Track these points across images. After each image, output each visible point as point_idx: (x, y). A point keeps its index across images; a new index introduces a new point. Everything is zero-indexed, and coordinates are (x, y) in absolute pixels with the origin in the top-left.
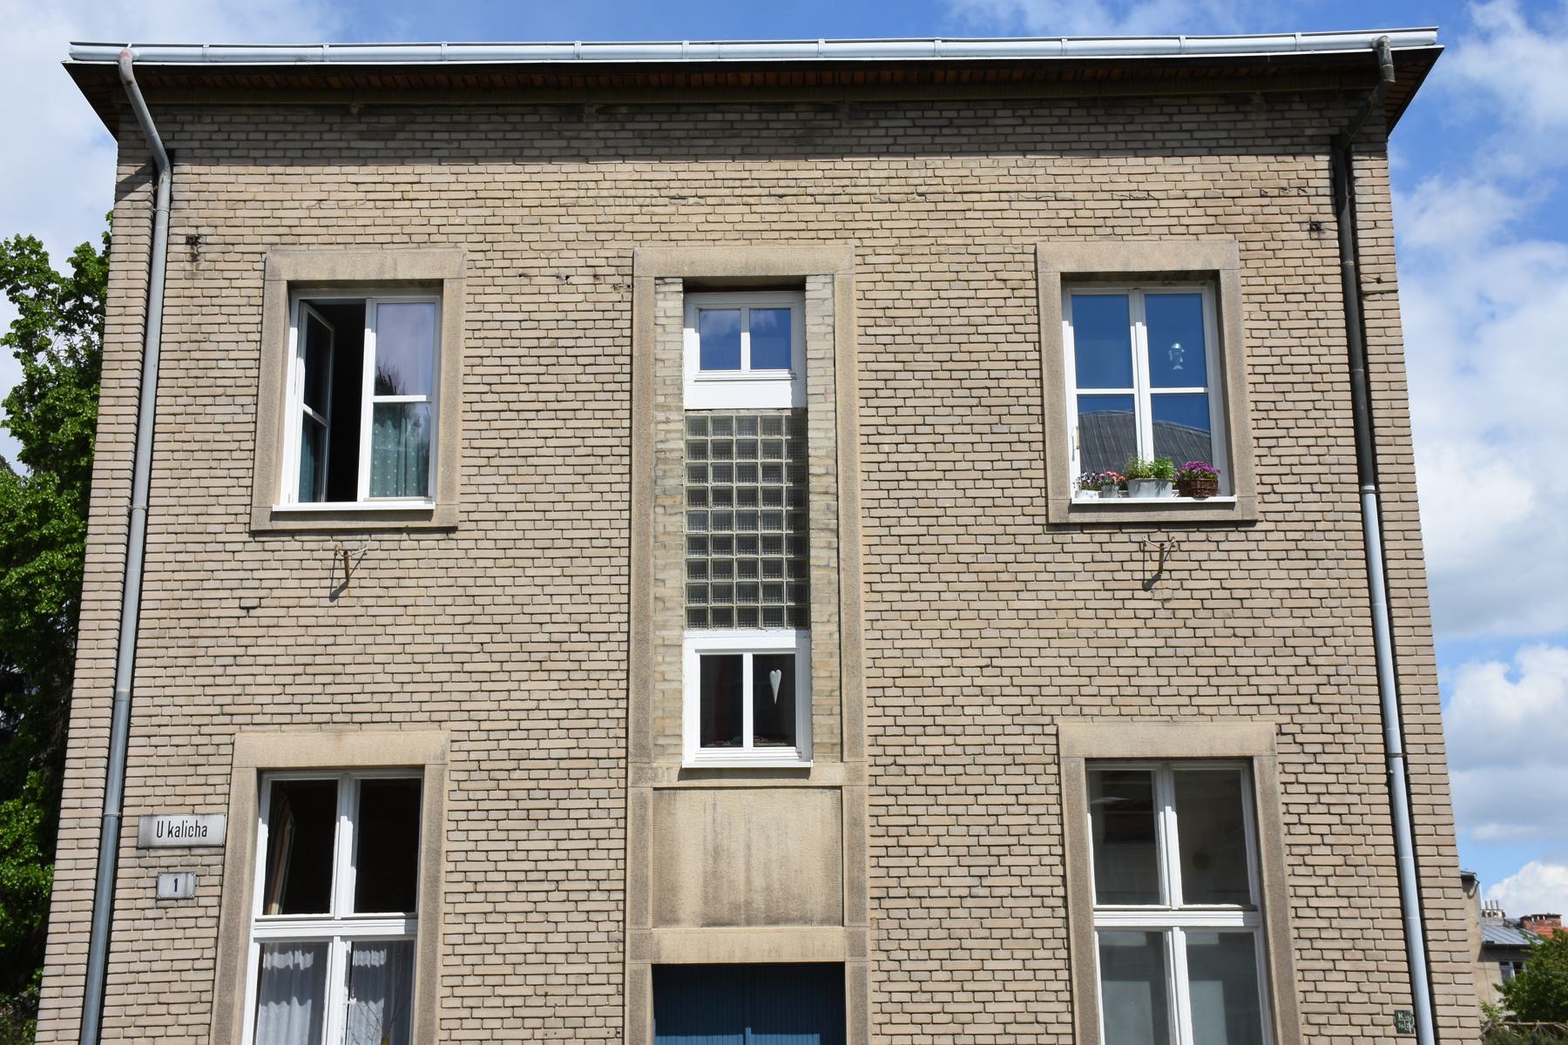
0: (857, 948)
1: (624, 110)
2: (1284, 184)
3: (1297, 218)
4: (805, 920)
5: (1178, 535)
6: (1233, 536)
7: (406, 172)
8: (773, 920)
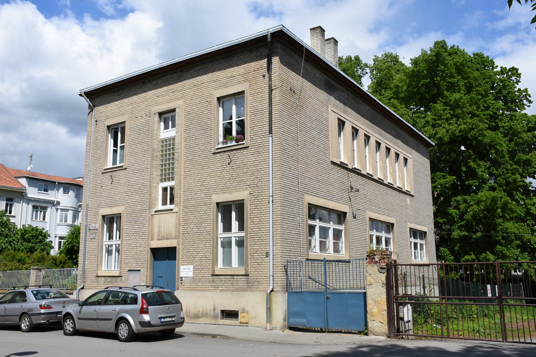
0: (179, 244)
2: (258, 67)
3: (260, 75)
4: (172, 239)
5: (235, 152)
6: (245, 151)
7: (122, 101)
8: (167, 239)
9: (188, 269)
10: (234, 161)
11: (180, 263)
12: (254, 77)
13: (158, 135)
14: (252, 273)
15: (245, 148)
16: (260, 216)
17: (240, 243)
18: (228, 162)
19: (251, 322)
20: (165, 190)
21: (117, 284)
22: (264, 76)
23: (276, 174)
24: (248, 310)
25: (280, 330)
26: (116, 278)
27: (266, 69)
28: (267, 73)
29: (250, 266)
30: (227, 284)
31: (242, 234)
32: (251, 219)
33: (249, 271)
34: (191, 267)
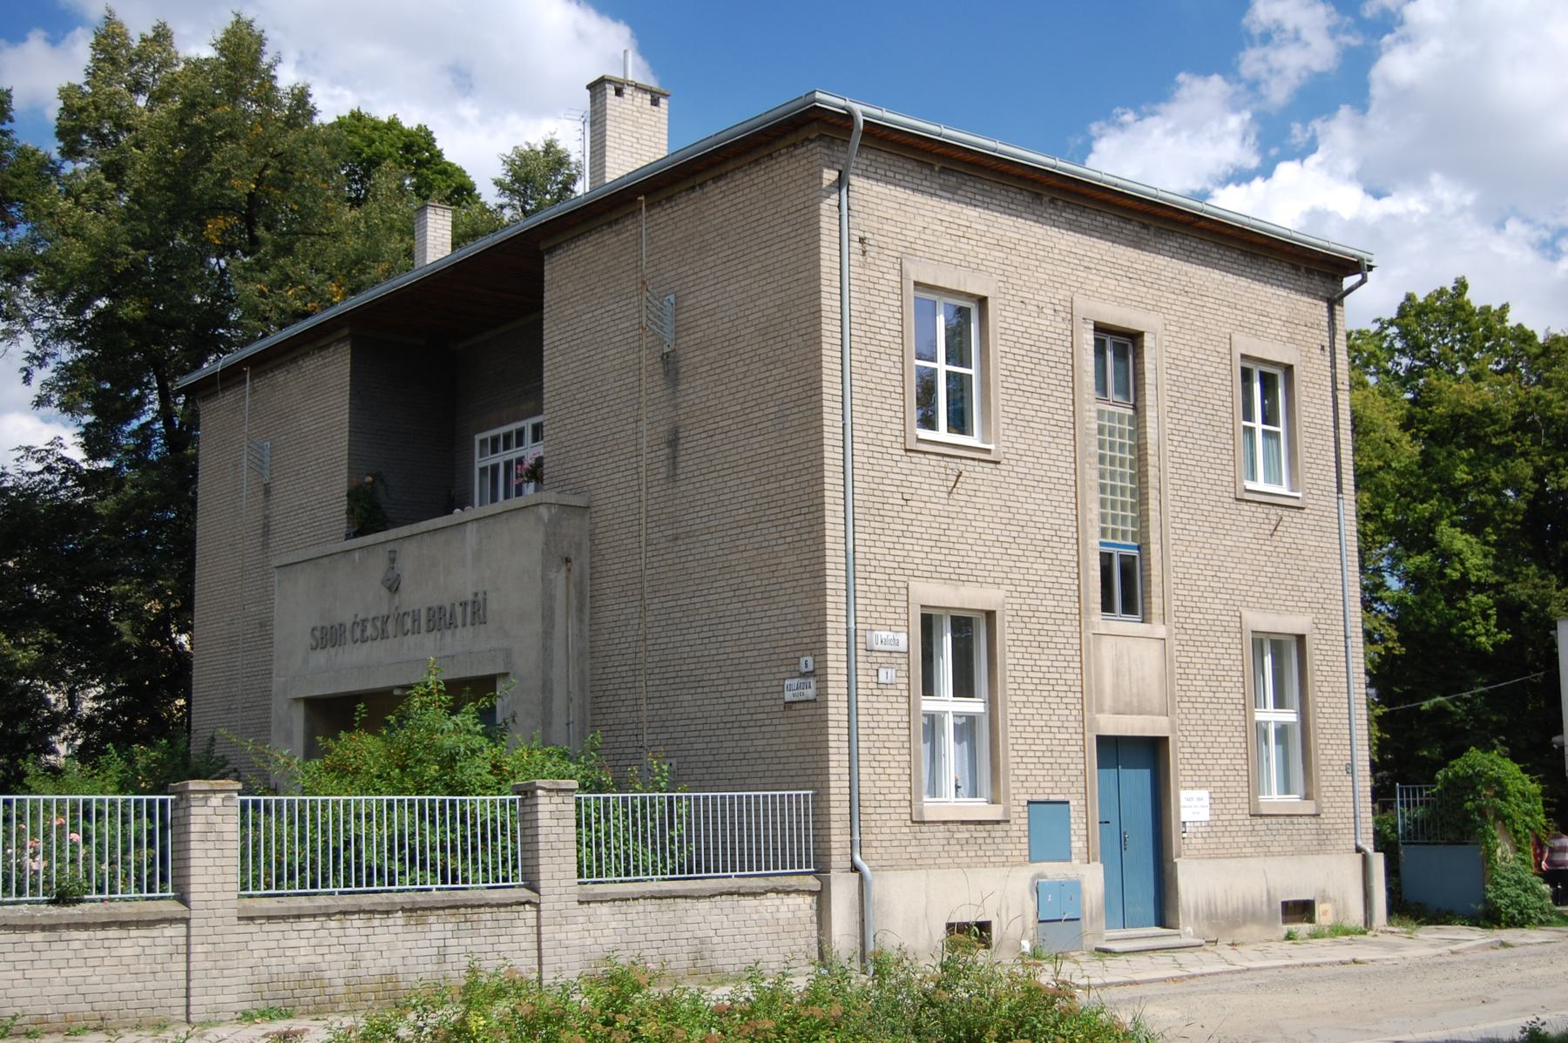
1: (1060, 203)
4: (1151, 713)
8: (1140, 713)
9: (1199, 799)
17: (967, 728)
26: (988, 827)
34: (1204, 794)
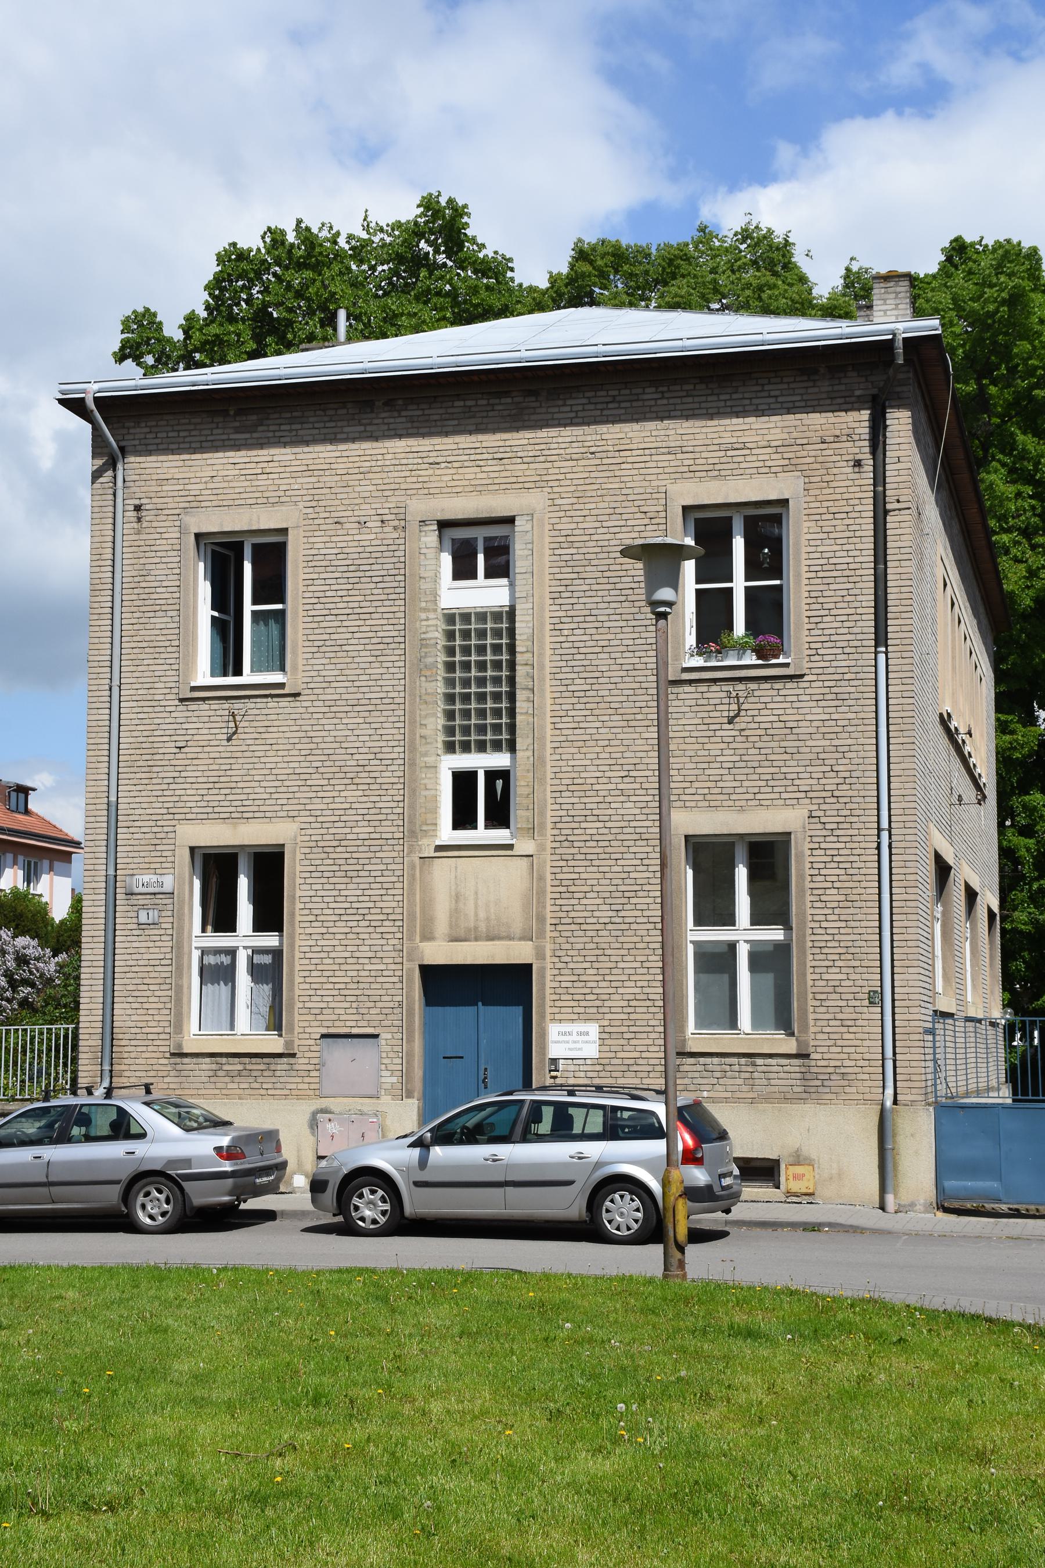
0: (540, 955)
2: (838, 433)
3: (845, 458)
5: (753, 686)
7: (264, 454)
9: (581, 1034)
10: (750, 713)
11: (548, 1017)
12: (820, 459)
13: (435, 595)
14: (819, 1049)
15: (791, 677)
16: (847, 885)
18: (726, 714)
19: (825, 1192)
20: (464, 782)
21: (274, 1080)
22: (858, 464)
23: (903, 766)
24: (814, 1156)
25: (926, 1212)
27: (867, 443)
28: (869, 456)
29: (812, 1029)
30: (731, 1081)
31: (775, 934)
32: (815, 892)
33: (812, 1043)
34: (593, 1029)
